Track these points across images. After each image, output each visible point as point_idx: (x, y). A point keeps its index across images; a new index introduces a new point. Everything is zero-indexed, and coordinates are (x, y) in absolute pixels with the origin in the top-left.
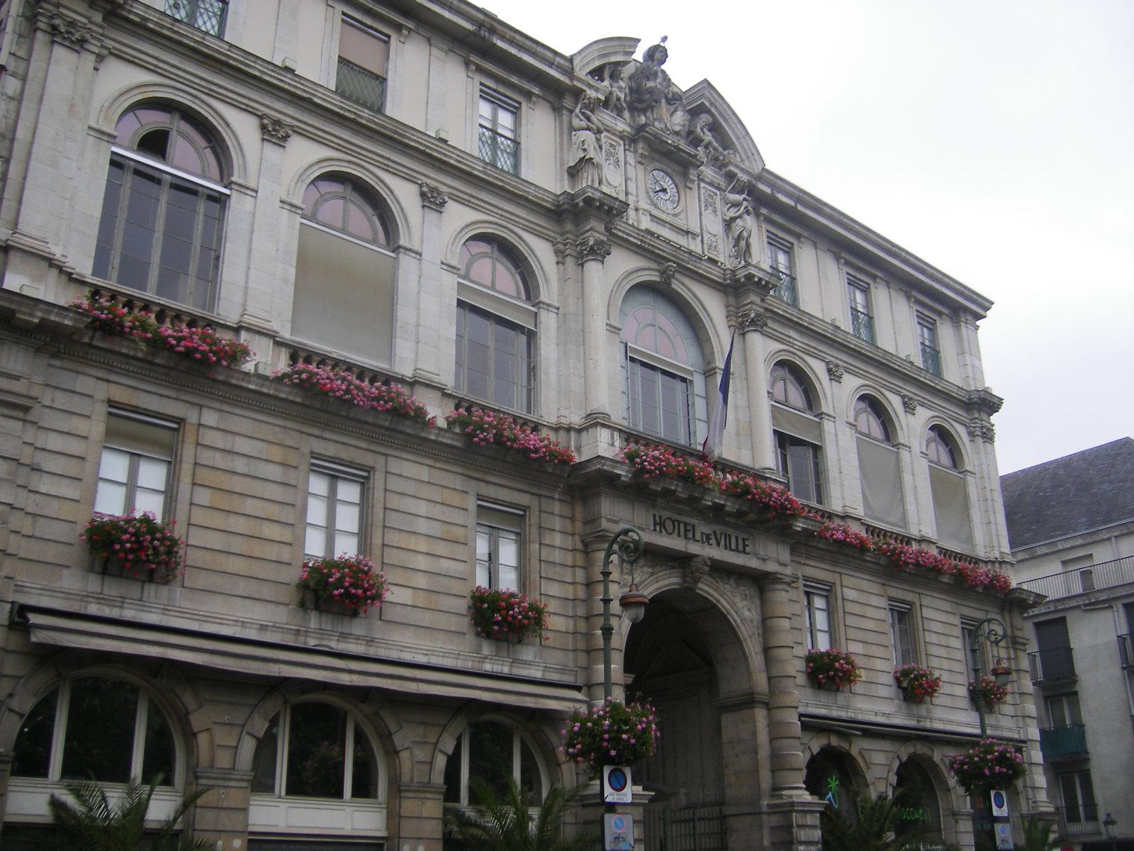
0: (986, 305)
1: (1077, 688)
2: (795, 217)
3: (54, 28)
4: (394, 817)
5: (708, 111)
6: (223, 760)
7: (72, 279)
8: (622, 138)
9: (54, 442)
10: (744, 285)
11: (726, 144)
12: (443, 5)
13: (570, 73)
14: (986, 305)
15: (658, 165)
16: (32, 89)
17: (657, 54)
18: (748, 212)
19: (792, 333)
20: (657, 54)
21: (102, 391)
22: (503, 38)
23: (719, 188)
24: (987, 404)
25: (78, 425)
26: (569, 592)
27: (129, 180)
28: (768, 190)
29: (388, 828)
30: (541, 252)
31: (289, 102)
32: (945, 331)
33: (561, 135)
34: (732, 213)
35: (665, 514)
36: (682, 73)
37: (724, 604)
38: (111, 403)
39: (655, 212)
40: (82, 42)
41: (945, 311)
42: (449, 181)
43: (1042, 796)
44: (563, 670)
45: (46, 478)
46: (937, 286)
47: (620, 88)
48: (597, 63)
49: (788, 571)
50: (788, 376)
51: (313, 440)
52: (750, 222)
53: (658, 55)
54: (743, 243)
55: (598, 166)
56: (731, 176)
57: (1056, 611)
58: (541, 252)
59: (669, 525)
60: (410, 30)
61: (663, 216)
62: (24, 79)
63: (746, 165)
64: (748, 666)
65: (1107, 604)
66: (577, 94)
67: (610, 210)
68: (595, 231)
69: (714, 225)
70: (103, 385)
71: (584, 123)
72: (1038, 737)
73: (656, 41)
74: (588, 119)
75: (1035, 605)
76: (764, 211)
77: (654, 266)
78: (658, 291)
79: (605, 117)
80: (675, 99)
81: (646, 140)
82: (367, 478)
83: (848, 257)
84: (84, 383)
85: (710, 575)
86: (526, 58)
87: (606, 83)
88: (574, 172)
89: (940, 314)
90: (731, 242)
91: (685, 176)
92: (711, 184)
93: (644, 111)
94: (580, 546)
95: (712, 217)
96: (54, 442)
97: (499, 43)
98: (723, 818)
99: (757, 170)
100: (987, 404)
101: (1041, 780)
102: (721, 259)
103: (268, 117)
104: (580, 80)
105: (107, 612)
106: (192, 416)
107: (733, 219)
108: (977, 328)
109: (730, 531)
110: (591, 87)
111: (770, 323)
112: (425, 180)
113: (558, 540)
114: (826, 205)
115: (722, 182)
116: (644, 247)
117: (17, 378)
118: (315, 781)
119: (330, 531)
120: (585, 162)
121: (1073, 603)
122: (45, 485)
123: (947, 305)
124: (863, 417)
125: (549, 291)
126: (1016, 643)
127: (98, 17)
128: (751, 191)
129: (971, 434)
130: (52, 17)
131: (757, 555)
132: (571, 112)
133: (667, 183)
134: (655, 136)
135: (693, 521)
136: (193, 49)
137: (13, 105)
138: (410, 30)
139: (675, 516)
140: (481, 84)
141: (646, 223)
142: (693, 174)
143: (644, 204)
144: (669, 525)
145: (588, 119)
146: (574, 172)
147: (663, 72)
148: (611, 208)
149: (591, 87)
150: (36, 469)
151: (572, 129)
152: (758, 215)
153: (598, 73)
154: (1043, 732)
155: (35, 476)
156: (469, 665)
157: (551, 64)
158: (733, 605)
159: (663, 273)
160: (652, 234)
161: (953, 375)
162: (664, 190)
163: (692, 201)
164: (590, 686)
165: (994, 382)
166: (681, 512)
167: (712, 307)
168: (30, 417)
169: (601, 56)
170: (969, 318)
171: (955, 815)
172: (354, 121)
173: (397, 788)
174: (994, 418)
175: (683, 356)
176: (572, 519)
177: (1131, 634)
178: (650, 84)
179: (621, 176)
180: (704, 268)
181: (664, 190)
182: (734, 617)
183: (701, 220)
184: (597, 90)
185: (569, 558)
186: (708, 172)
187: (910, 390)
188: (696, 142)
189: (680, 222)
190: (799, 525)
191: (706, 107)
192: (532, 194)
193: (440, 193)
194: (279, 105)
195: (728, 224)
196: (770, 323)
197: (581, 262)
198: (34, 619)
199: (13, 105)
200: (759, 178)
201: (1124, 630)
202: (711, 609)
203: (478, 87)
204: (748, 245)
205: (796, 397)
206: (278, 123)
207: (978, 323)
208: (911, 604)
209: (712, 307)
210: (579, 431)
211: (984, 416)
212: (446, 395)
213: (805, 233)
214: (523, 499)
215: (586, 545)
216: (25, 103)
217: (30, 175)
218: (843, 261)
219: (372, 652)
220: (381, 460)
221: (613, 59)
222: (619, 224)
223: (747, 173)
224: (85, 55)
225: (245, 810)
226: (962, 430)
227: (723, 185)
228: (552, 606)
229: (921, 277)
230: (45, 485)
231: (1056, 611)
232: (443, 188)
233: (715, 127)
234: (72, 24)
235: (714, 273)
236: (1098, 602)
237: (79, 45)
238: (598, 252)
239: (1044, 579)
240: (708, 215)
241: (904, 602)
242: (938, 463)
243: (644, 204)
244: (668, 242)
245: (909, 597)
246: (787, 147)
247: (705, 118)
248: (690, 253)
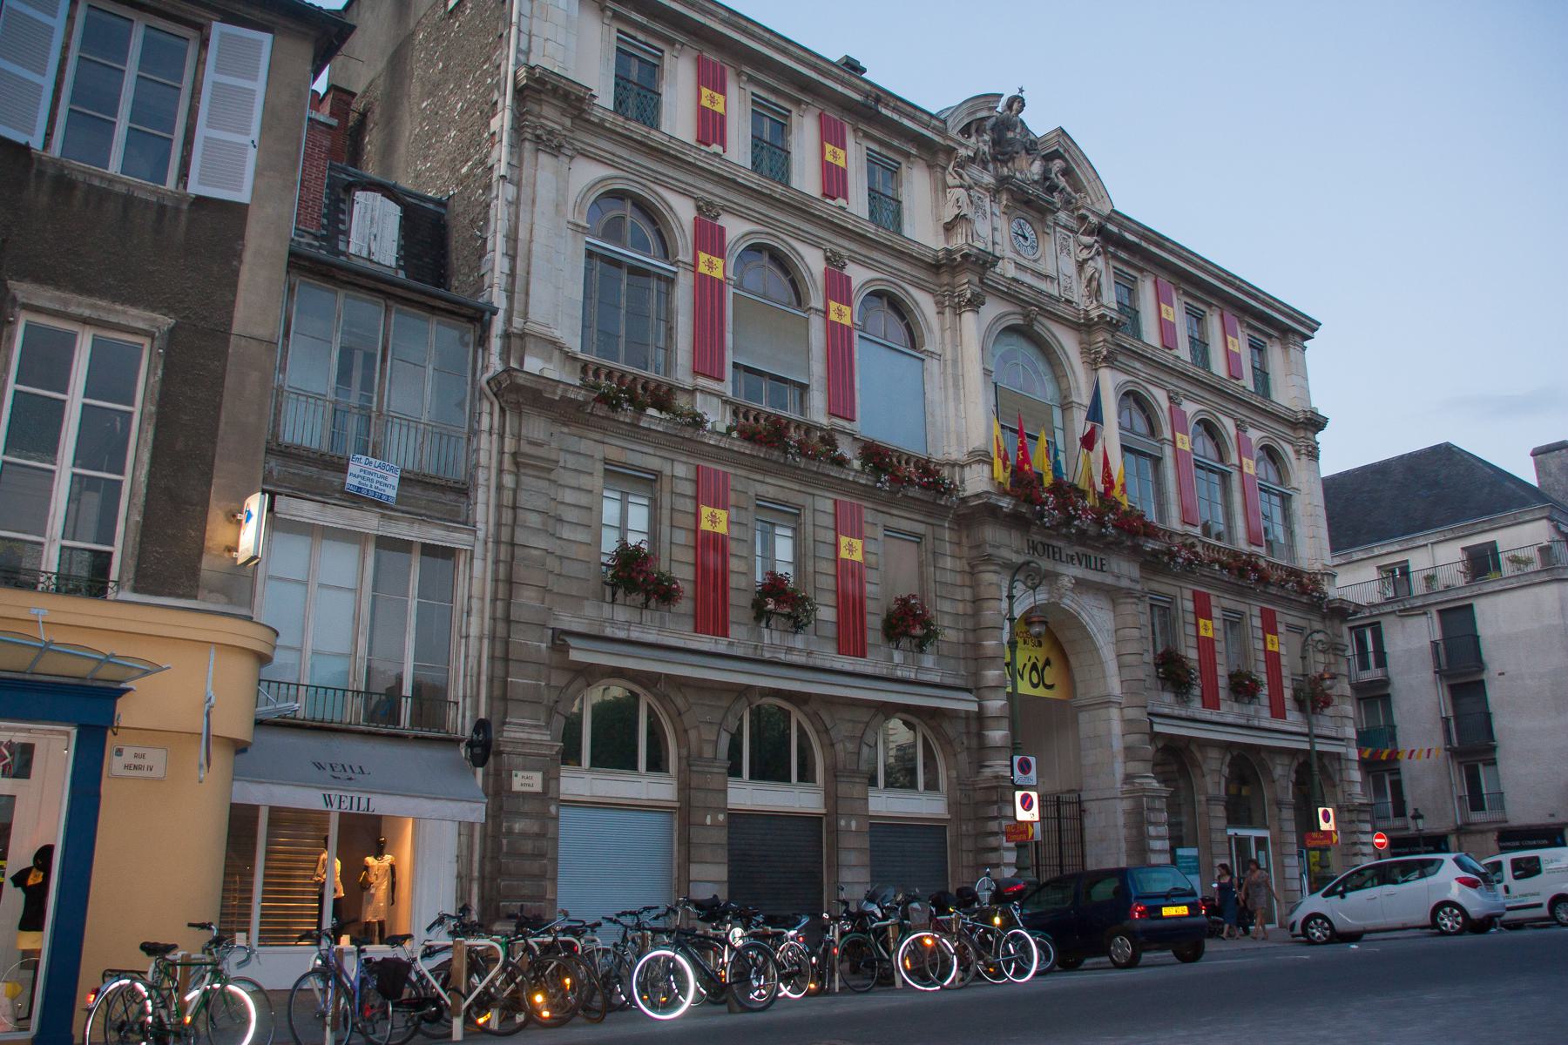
0: (1313, 326)
1: (1389, 691)
2: (1133, 249)
3: (538, 137)
4: (832, 798)
5: (1061, 157)
6: (708, 752)
7: (570, 357)
8: (987, 190)
9: (569, 496)
10: (1097, 323)
11: (1078, 188)
12: (692, 6)
13: (943, 132)
14: (1313, 326)
15: (1019, 213)
16: (526, 192)
17: (1017, 102)
18: (1098, 254)
19: (1138, 365)
20: (1017, 102)
21: (599, 451)
22: (887, 106)
23: (1072, 231)
24: (1316, 423)
25: (585, 481)
26: (960, 608)
27: (598, 264)
28: (1115, 230)
29: (826, 806)
30: (924, 303)
31: (717, 183)
32: (1275, 353)
33: (936, 190)
34: (1085, 254)
35: (1037, 538)
36: (1038, 122)
37: (1085, 618)
38: (606, 461)
39: (1019, 259)
40: (560, 146)
41: (1276, 334)
42: (846, 243)
43: (1358, 789)
44: (956, 676)
45: (566, 527)
46: (1268, 311)
47: (985, 142)
48: (966, 121)
49: (1138, 587)
50: (1134, 405)
51: (758, 485)
52: (1100, 262)
53: (1015, 106)
54: (1094, 284)
55: (969, 221)
56: (1083, 218)
57: (1372, 616)
58: (924, 303)
59: (1040, 547)
60: (683, 44)
61: (1025, 262)
62: (518, 185)
63: (1097, 207)
64: (1104, 671)
65: (1422, 610)
66: (950, 151)
67: (983, 262)
68: (966, 283)
69: (1069, 267)
70: (600, 446)
71: (958, 181)
72: (1354, 736)
73: (1016, 93)
74: (961, 176)
75: (1355, 613)
76: (1111, 249)
77: (1018, 310)
78: (1024, 332)
79: (975, 171)
80: (1031, 146)
81: (1008, 190)
82: (798, 515)
83: (1187, 288)
84: (585, 446)
85: (1072, 590)
86: (1153, 249)
87: (973, 139)
88: (949, 228)
89: (1270, 336)
90: (1084, 282)
91: (1043, 221)
92: (1065, 227)
93: (1004, 163)
94: (967, 568)
95: (1066, 259)
96: (569, 496)
97: (884, 111)
98: (1080, 802)
99: (1107, 211)
100: (1316, 423)
101: (1356, 775)
102: (1076, 299)
103: (702, 199)
104: (952, 139)
105: (622, 634)
106: (667, 470)
107: (1085, 261)
108: (1304, 348)
109: (1090, 552)
110: (961, 145)
111: (1120, 358)
112: (702, 194)
113: (948, 563)
114: (1167, 240)
115: (1074, 224)
116: (1010, 293)
117: (541, 445)
118: (770, 768)
119: (623, 528)
120: (960, 218)
121: (1388, 609)
122: (567, 533)
123: (1281, 327)
124: (1199, 440)
125: (932, 342)
126: (1335, 648)
127: (568, 123)
128: (1100, 231)
129: (1297, 452)
130: (535, 128)
131: (1113, 574)
132: (944, 169)
133: (1028, 231)
134: (1019, 187)
135: (1060, 544)
136: (640, 143)
137: (513, 209)
138: (683, 44)
139: (1045, 540)
140: (619, 31)
141: (1011, 272)
142: (1050, 219)
143: (1009, 253)
144: (1040, 547)
145: (961, 176)
146: (949, 228)
147: (1022, 122)
148: (985, 262)
149: (961, 145)
150: (560, 520)
151: (946, 186)
152: (1105, 253)
153: (966, 131)
154: (1358, 733)
155: (558, 526)
156: (884, 672)
157: (927, 126)
158: (1092, 617)
159: (1026, 316)
160: (1016, 281)
161: (1283, 396)
162: (1026, 238)
163: (1049, 246)
164: (978, 689)
165: (1321, 403)
166: (1050, 536)
167: (1068, 343)
168: (552, 477)
169: (969, 114)
170: (1298, 339)
171: (1279, 804)
172: (770, 196)
173: (834, 773)
174: (1319, 437)
175: (1045, 391)
176: (959, 544)
177: (1444, 639)
178: (1010, 135)
179: (993, 229)
180: (1061, 310)
181: (1026, 238)
182: (1092, 628)
183: (1060, 264)
184: (967, 147)
185: (958, 579)
186: (1063, 216)
187: (1243, 412)
188: (1052, 189)
189: (1039, 267)
190: (1150, 545)
191: (1060, 155)
192: (1283, 413)
193: (841, 257)
194: (709, 187)
195: (1081, 265)
196: (1120, 358)
197: (957, 310)
198: (572, 642)
199: (513, 209)
200: (1109, 219)
201: (1438, 636)
202: (1073, 620)
203: (615, 34)
204: (1099, 285)
205: (1140, 424)
206: (710, 204)
207: (1306, 343)
208: (1242, 614)
209: (1068, 343)
210: (962, 467)
211: (1310, 435)
212: (855, 439)
213: (681, 38)
214: (920, 528)
215: (972, 567)
216: (522, 207)
217: (533, 270)
218: (609, 14)
219: (811, 662)
220: (810, 499)
221: (979, 115)
222: (989, 274)
223: (1098, 215)
224: (562, 158)
225: (725, 792)
226: (1288, 448)
227: (1075, 227)
228: (946, 621)
229: (1253, 303)
230: (567, 533)
231: (1372, 616)
232: (843, 252)
233: (1067, 172)
234: (551, 132)
235: (1067, 312)
236: (1413, 608)
237: (556, 151)
238: (975, 303)
239: (1357, 582)
240: (1063, 258)
241: (1235, 612)
242: (1132, 430)
243: (1009, 253)
244: (1030, 287)
245: (1241, 607)
246: (1133, 189)
247: (1057, 164)
248: (1050, 296)
